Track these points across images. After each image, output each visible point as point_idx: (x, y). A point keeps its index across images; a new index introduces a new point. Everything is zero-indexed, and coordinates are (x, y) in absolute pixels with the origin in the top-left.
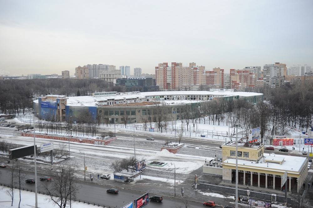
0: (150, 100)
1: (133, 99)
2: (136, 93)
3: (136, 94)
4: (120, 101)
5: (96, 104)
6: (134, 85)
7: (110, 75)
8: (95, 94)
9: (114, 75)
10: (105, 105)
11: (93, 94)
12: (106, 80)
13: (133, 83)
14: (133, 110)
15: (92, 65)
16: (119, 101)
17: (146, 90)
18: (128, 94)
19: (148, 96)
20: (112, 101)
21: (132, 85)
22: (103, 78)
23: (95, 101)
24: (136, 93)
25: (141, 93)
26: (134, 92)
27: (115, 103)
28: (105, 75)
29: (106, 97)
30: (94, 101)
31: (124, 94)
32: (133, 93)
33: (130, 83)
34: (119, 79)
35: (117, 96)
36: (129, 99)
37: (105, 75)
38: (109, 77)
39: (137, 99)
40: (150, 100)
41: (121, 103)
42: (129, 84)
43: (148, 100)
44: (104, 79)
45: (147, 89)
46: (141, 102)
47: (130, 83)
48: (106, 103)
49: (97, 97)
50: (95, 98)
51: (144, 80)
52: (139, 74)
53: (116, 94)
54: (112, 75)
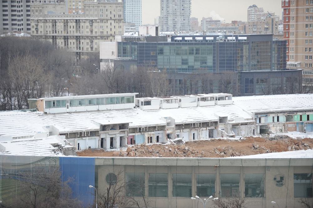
0: (275, 132)
1: (205, 124)
2: (212, 99)
3: (213, 103)
4: (154, 134)
5: (55, 145)
6: (198, 65)
7: (77, 22)
8: (50, 104)
9: (95, 24)
10: (90, 151)
11: (39, 104)
12: (60, 42)
13: (191, 59)
14: (252, 175)
15: (265, 12)
16: (147, 135)
17: (246, 87)
18: (183, 104)
19: (267, 114)
20: (117, 135)
21: (185, 67)
22: (46, 37)
23: (51, 134)
24: (212, 99)
25: (236, 99)
26: (205, 95)
27: (132, 141)
28: (54, 22)
29: (95, 115)
30: (48, 131)
31: (165, 105)
32: (204, 99)
33: (179, 59)
34: (128, 41)
35: (138, 110)
36: (187, 126)
37: (54, 22)
38: (72, 31)
39: (221, 127)
40: (275, 132)
41: (154, 140)
42: (176, 62)
43: (263, 131)
44: (54, 38)
45: (252, 81)
46: (237, 138)
47: (179, 59)
48: (94, 143)
49: (57, 117)
50: (49, 121)
51: (239, 44)
52: (179, 20)
53: (132, 105)
54: (88, 24)
